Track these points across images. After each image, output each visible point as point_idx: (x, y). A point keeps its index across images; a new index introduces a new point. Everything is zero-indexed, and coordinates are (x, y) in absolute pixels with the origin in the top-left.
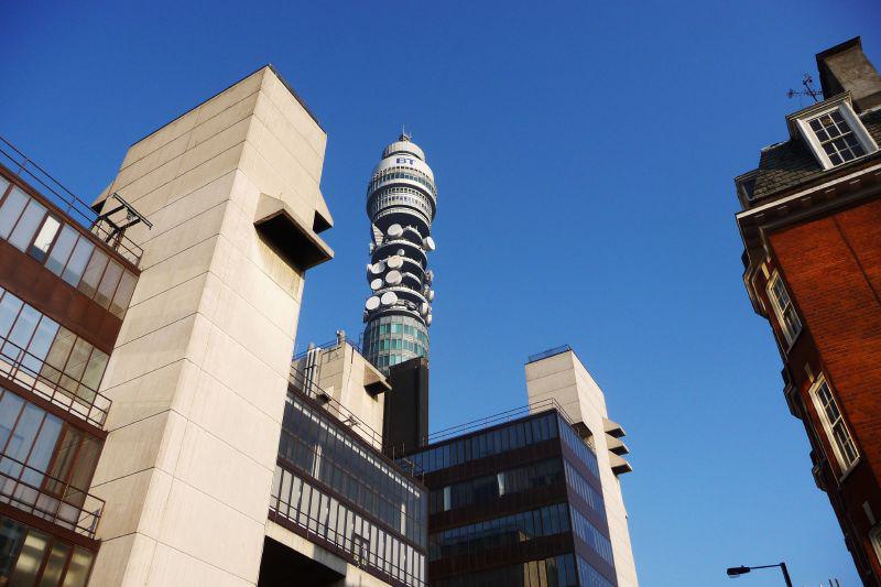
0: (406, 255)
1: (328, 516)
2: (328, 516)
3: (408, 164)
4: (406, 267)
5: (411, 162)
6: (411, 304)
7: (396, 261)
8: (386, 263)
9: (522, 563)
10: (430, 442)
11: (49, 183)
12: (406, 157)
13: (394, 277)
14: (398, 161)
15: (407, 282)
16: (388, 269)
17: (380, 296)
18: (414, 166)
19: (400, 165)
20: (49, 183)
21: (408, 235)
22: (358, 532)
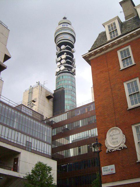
0: (67, 54)
1: (18, 137)
2: (18, 137)
3: (66, 26)
4: (67, 58)
5: (67, 26)
6: (69, 69)
7: (64, 56)
8: (61, 57)
9: (69, 136)
10: (77, 107)
11: (6, 99)
12: (65, 24)
13: (63, 61)
14: (63, 26)
15: (67, 62)
16: (61, 59)
17: (60, 67)
18: (68, 27)
19: (63, 27)
20: (6, 99)
21: (67, 48)
22: (28, 140)
